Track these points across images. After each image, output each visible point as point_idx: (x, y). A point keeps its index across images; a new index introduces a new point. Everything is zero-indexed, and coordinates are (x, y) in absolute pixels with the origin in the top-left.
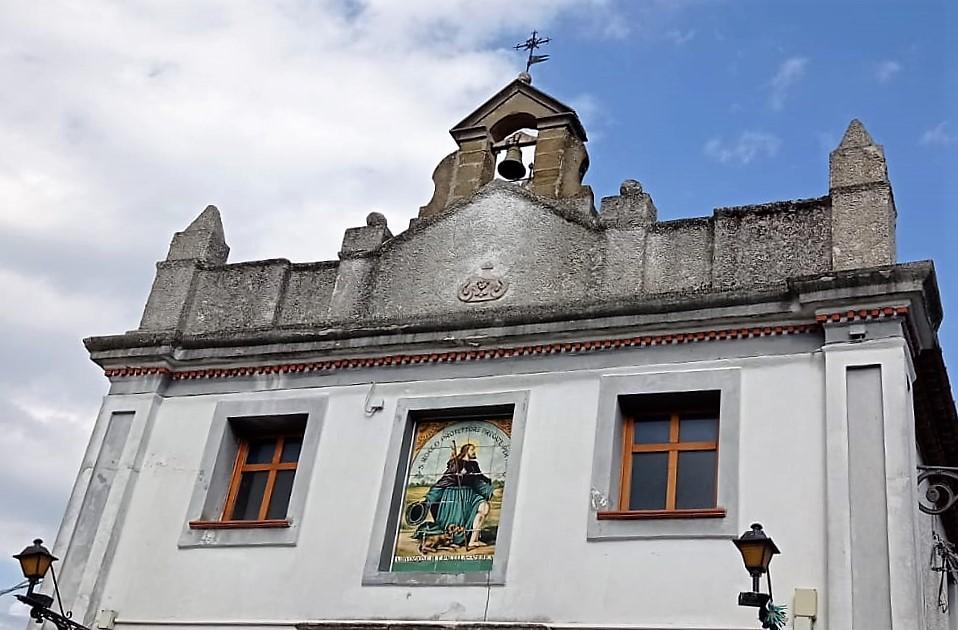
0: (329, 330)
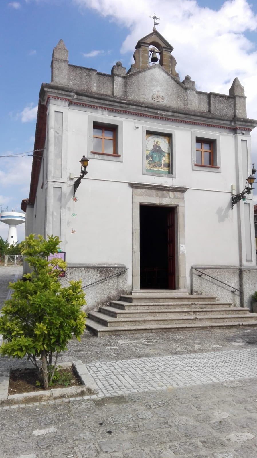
0: (125, 101)
